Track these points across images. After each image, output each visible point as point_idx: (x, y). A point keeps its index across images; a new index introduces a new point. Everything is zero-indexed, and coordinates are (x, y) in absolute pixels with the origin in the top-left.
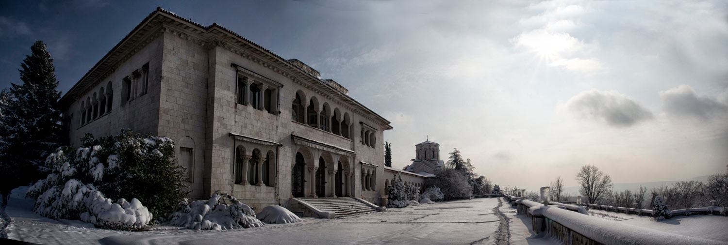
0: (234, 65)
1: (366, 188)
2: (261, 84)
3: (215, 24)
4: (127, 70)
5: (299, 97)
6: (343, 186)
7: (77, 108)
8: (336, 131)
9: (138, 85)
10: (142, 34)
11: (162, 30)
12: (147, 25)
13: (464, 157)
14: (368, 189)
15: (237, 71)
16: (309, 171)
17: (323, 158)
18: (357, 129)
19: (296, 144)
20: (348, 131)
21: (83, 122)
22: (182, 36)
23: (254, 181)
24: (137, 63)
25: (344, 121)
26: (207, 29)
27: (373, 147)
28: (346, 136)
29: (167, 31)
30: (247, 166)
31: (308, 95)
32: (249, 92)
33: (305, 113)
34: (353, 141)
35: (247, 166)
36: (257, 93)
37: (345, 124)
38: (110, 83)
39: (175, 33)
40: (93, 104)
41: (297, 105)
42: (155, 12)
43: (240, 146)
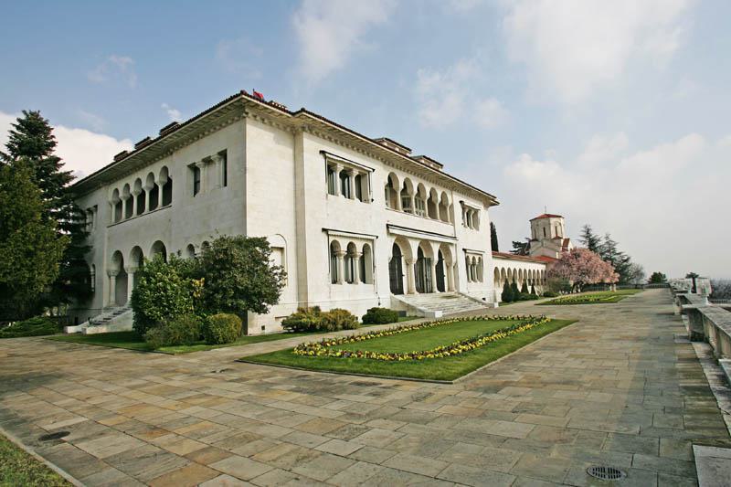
0: (322, 152)
1: (344, 193)
2: (351, 170)
3: (303, 110)
4: (194, 153)
5: (391, 182)
6: (445, 278)
7: (103, 199)
8: (432, 215)
9: (210, 176)
10: (217, 116)
11: (244, 115)
12: (225, 108)
13: (599, 233)
14: (474, 281)
15: (326, 157)
16: (407, 264)
17: (398, 243)
18: (458, 210)
19: (392, 234)
20: (446, 213)
21: (118, 218)
22: (266, 121)
23: (350, 278)
24: (208, 146)
25: (441, 202)
26: (293, 114)
27: (478, 230)
28: (444, 220)
29: (250, 115)
30: (341, 262)
31: (401, 178)
32: (338, 181)
33: (399, 197)
34: (453, 224)
35: (341, 262)
36: (346, 180)
37: (443, 206)
38: (165, 169)
39: (258, 118)
40: (136, 194)
41: (388, 189)
42: (237, 96)
43: (334, 242)
